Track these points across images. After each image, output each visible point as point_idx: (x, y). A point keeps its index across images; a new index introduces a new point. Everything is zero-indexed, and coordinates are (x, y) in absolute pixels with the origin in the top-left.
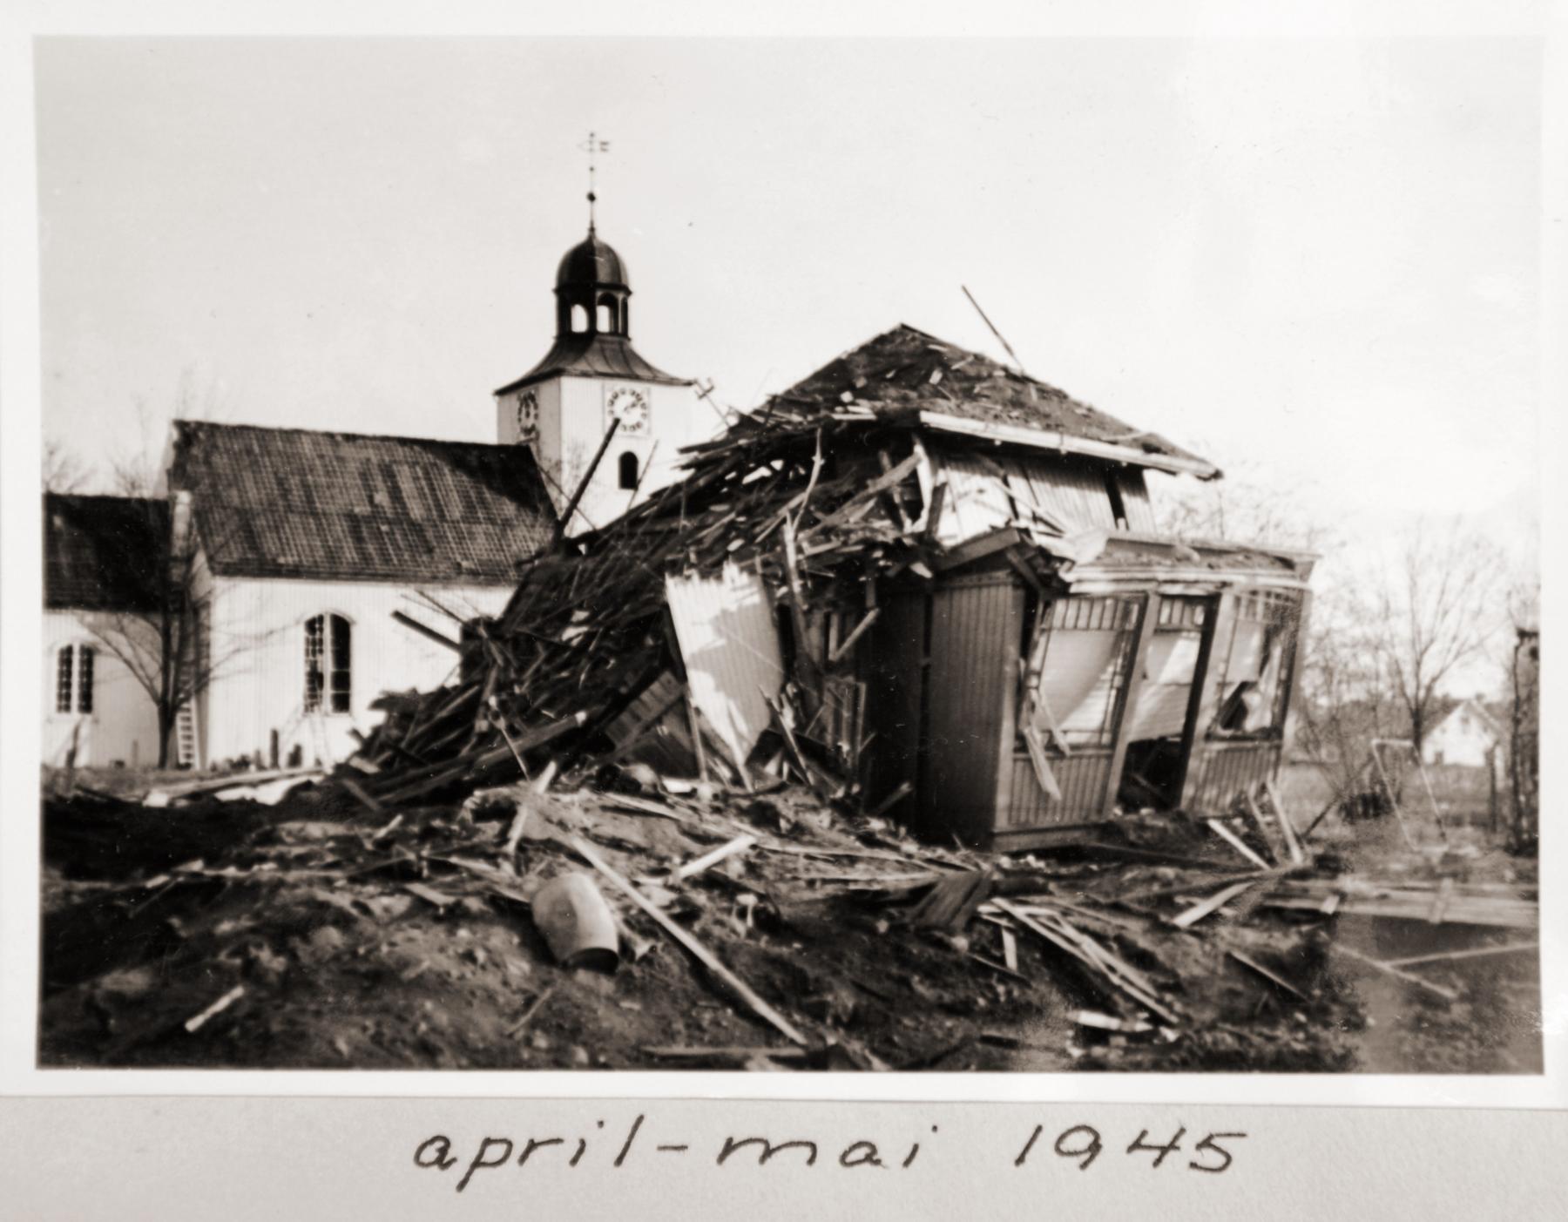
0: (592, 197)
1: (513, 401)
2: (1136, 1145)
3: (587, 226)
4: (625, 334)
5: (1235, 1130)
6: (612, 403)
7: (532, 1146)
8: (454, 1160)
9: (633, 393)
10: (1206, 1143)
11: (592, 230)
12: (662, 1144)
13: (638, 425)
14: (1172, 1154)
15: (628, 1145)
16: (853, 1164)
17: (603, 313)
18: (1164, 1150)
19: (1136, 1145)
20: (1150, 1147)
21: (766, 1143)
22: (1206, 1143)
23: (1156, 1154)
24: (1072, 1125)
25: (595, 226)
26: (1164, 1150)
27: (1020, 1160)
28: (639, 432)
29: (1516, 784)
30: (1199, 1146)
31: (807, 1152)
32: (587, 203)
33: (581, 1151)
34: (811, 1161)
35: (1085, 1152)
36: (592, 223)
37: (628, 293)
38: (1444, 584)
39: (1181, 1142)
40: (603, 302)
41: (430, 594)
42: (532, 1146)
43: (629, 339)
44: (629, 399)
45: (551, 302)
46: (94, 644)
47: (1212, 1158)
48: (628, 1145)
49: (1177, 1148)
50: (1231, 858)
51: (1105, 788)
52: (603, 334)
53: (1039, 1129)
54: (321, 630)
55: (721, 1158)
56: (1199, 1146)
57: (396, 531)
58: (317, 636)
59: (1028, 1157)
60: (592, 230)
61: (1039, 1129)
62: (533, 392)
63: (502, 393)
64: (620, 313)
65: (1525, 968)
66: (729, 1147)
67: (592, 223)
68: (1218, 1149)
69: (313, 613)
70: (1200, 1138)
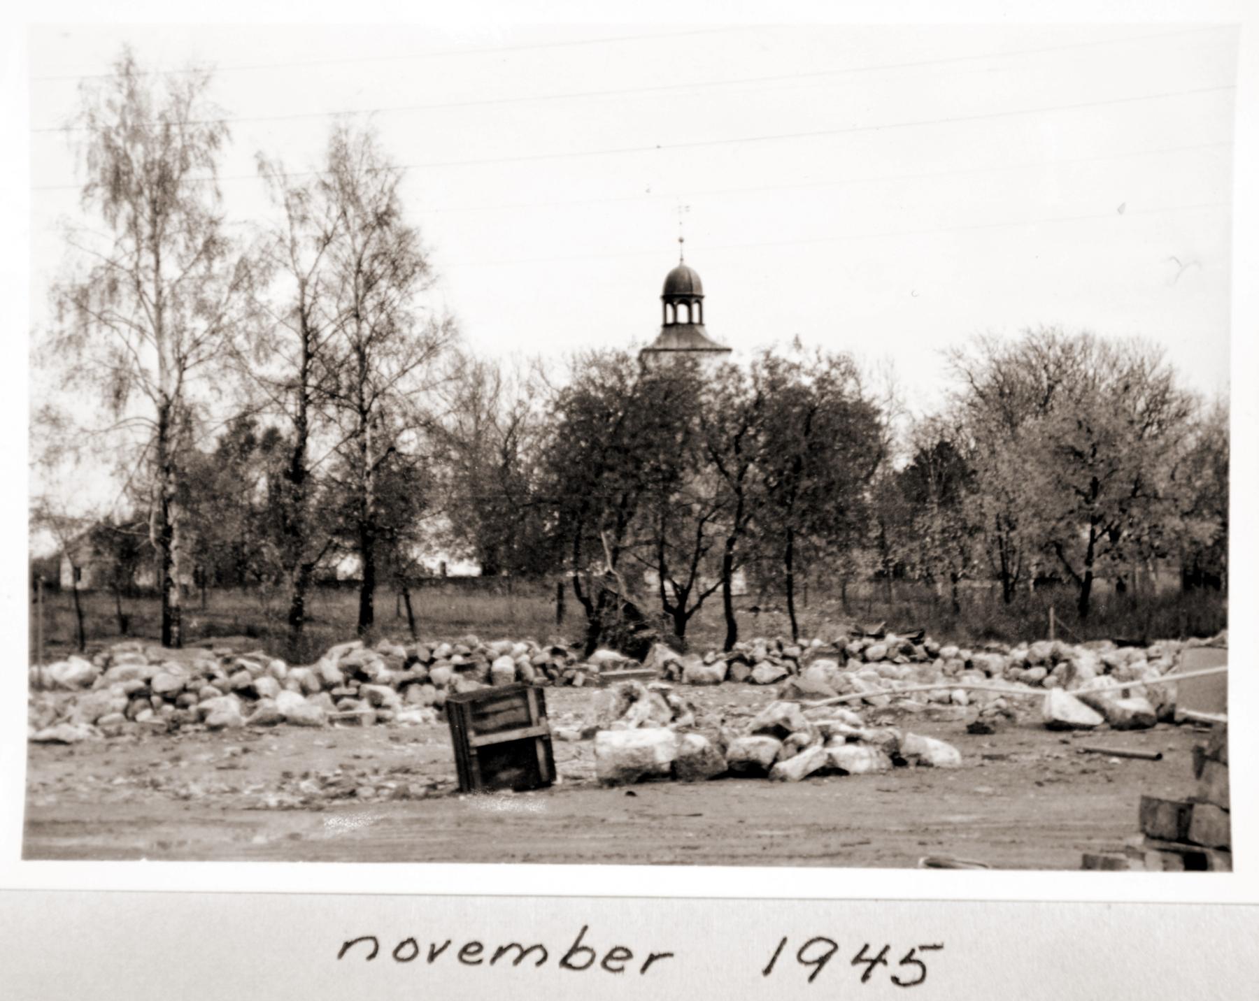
0: (681, 241)
5: (930, 943)
7: (652, 958)
10: (907, 960)
14: (879, 966)
15: (773, 960)
18: (874, 962)
19: (857, 960)
20: (867, 960)
21: (519, 946)
22: (907, 960)
24: (806, 940)
27: (767, 971)
29: (292, 251)
30: (903, 962)
33: (348, 945)
34: (372, 956)
35: (814, 962)
39: (887, 956)
42: (652, 958)
46: (648, 661)
48: (773, 960)
49: (885, 962)
50: (80, 526)
51: (1209, 645)
53: (784, 940)
55: (341, 954)
56: (903, 962)
57: (371, 478)
61: (784, 940)
65: (1224, 731)
66: (348, 945)
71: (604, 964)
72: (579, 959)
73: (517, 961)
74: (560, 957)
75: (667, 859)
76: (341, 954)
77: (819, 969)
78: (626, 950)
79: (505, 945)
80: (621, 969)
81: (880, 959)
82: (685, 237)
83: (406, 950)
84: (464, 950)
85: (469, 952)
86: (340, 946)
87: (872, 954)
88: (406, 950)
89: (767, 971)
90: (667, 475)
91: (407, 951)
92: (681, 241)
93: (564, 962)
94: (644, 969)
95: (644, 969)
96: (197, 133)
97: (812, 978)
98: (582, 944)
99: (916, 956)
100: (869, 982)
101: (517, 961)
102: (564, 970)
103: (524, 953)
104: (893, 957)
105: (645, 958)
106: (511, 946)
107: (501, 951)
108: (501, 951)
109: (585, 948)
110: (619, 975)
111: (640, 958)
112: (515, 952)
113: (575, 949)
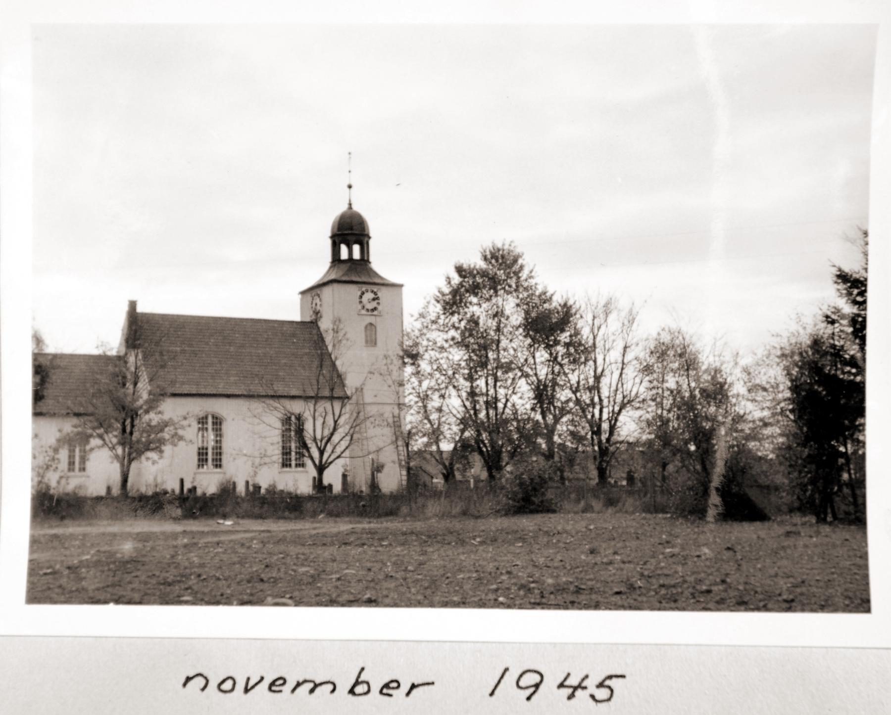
0: (350, 187)
1: (308, 297)
2: (561, 685)
3: (348, 202)
4: (368, 261)
6: (361, 297)
7: (413, 686)
8: (390, 695)
9: (372, 291)
10: (601, 685)
11: (350, 204)
12: (430, 687)
13: (375, 309)
16: (274, 691)
17: (356, 248)
18: (575, 688)
19: (561, 685)
21: (313, 682)
22: (601, 685)
23: (570, 691)
25: (352, 202)
26: (575, 688)
27: (492, 694)
28: (375, 313)
31: (331, 687)
32: (348, 189)
36: (350, 201)
37: (369, 238)
38: (623, 361)
40: (356, 242)
41: (501, 410)
42: (413, 686)
43: (370, 263)
44: (371, 296)
45: (328, 244)
47: (602, 694)
52: (357, 260)
54: (207, 423)
55: (185, 685)
58: (205, 426)
59: (496, 692)
60: (350, 204)
62: (319, 292)
63: (303, 293)
64: (365, 250)
66: (188, 679)
67: (350, 201)
68: (527, 688)
69: (202, 414)
70: (597, 682)
71: (381, 692)
72: (359, 689)
73: (312, 691)
74: (349, 687)
75: (213, 601)
76: (185, 685)
77: (534, 692)
78: (397, 681)
79: (301, 680)
80: (280, 691)
81: (580, 687)
82: (353, 184)
83: (226, 685)
84: (273, 684)
85: (276, 685)
86: (183, 680)
87: (573, 681)
88: (226, 685)
89: (492, 694)
90: (447, 381)
91: (228, 685)
92: (350, 187)
93: (352, 691)
94: (408, 694)
95: (408, 694)
96: (705, 438)
97: (529, 698)
98: (360, 680)
99: (608, 683)
100: (494, 697)
101: (312, 691)
102: (350, 696)
103: (316, 686)
104: (591, 683)
105: (295, 684)
106: (305, 681)
107: (298, 684)
108: (298, 684)
109: (363, 682)
110: (279, 695)
111: (405, 688)
112: (311, 685)
113: (357, 683)
